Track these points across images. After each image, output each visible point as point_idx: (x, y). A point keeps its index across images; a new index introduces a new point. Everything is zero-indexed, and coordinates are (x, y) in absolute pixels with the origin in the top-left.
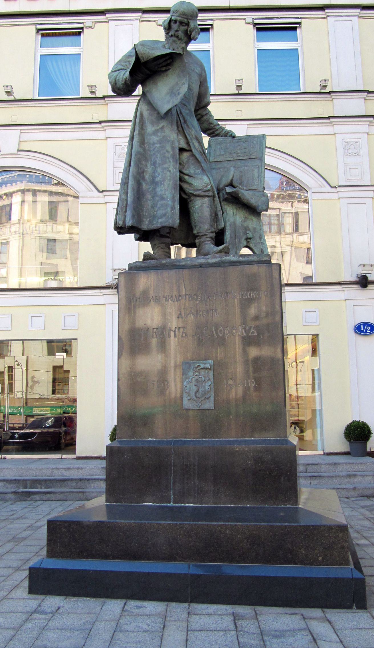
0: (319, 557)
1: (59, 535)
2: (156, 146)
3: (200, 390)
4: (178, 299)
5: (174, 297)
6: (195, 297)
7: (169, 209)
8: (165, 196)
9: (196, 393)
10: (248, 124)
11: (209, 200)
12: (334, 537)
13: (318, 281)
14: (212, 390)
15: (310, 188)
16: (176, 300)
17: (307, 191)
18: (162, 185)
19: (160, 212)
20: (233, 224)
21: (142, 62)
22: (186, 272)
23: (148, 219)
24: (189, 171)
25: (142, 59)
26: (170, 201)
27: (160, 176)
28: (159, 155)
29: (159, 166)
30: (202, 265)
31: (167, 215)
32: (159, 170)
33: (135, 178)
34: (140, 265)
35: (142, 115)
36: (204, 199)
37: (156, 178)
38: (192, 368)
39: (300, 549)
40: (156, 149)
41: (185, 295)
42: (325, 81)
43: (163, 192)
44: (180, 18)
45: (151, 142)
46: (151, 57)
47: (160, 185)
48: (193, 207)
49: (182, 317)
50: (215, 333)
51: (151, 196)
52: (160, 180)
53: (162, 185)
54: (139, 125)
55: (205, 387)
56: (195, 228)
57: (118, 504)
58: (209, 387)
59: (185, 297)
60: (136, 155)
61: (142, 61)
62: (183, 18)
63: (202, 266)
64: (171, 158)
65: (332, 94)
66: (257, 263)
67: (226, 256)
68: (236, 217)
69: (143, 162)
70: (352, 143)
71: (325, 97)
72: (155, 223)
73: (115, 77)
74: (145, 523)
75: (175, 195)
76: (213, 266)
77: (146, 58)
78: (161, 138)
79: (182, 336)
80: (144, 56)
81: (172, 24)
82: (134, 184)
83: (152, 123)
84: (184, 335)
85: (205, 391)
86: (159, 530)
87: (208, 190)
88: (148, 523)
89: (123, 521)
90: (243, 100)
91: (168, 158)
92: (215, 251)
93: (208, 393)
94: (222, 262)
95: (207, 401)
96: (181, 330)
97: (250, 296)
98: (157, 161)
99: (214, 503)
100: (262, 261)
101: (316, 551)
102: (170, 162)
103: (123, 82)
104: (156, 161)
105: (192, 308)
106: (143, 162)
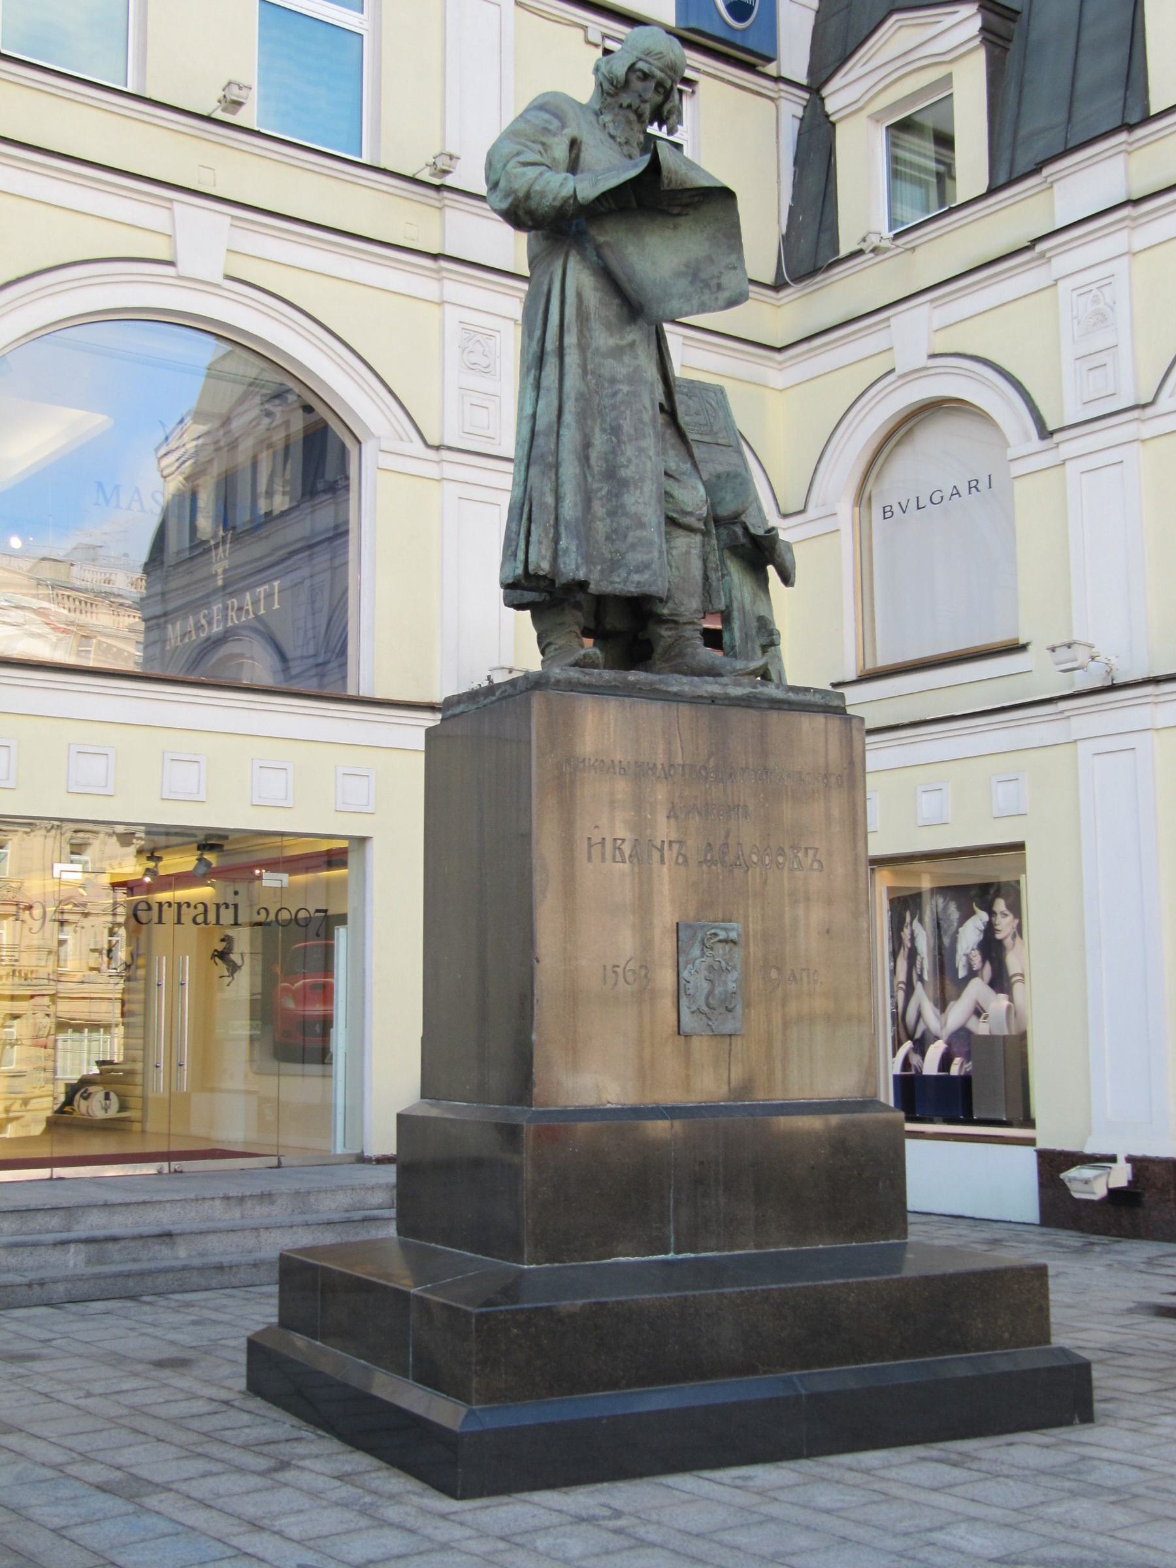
1: (503, 1347)
3: (716, 992)
4: (667, 771)
5: (659, 767)
6: (703, 773)
8: (645, 520)
9: (707, 998)
10: (233, 217)
15: (371, 435)
16: (663, 775)
17: (359, 442)
18: (639, 491)
19: (635, 558)
22: (684, 709)
23: (599, 567)
25: (666, 181)
27: (632, 467)
28: (628, 412)
30: (716, 698)
31: (653, 566)
34: (578, 678)
36: (692, 535)
37: (622, 469)
38: (699, 939)
41: (683, 766)
42: (240, 88)
45: (606, 372)
46: (688, 186)
49: (676, 818)
51: (604, 510)
53: (639, 491)
55: (725, 983)
59: (683, 770)
61: (665, 186)
63: (716, 702)
65: (446, 194)
66: (821, 709)
70: (479, 337)
71: (427, 196)
72: (617, 579)
73: (531, 181)
74: (694, 1296)
76: (738, 705)
79: (677, 863)
83: (608, 326)
84: (681, 860)
85: (726, 991)
88: (701, 1295)
89: (648, 1296)
90: (221, 140)
92: (741, 670)
93: (732, 997)
94: (755, 697)
95: (730, 1015)
96: (675, 847)
99: (758, 1246)
100: (831, 706)
101: (1000, 1322)
103: (557, 203)
104: (619, 427)
105: (697, 797)
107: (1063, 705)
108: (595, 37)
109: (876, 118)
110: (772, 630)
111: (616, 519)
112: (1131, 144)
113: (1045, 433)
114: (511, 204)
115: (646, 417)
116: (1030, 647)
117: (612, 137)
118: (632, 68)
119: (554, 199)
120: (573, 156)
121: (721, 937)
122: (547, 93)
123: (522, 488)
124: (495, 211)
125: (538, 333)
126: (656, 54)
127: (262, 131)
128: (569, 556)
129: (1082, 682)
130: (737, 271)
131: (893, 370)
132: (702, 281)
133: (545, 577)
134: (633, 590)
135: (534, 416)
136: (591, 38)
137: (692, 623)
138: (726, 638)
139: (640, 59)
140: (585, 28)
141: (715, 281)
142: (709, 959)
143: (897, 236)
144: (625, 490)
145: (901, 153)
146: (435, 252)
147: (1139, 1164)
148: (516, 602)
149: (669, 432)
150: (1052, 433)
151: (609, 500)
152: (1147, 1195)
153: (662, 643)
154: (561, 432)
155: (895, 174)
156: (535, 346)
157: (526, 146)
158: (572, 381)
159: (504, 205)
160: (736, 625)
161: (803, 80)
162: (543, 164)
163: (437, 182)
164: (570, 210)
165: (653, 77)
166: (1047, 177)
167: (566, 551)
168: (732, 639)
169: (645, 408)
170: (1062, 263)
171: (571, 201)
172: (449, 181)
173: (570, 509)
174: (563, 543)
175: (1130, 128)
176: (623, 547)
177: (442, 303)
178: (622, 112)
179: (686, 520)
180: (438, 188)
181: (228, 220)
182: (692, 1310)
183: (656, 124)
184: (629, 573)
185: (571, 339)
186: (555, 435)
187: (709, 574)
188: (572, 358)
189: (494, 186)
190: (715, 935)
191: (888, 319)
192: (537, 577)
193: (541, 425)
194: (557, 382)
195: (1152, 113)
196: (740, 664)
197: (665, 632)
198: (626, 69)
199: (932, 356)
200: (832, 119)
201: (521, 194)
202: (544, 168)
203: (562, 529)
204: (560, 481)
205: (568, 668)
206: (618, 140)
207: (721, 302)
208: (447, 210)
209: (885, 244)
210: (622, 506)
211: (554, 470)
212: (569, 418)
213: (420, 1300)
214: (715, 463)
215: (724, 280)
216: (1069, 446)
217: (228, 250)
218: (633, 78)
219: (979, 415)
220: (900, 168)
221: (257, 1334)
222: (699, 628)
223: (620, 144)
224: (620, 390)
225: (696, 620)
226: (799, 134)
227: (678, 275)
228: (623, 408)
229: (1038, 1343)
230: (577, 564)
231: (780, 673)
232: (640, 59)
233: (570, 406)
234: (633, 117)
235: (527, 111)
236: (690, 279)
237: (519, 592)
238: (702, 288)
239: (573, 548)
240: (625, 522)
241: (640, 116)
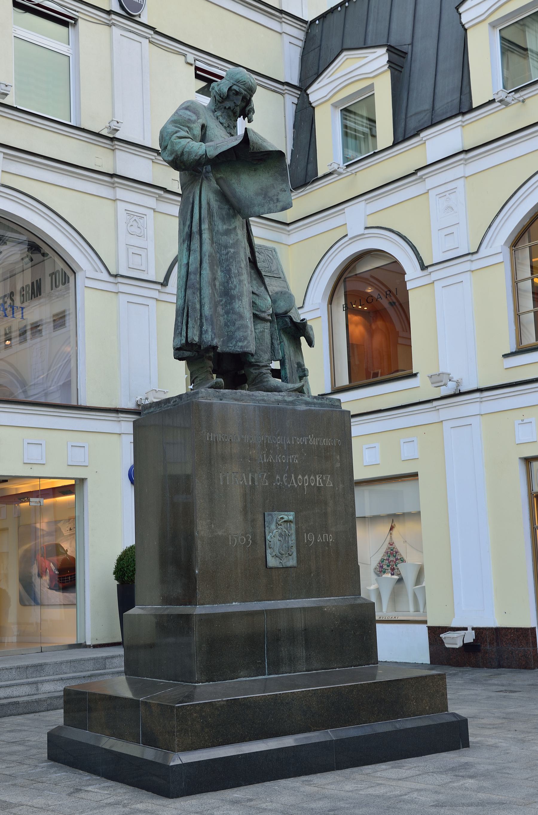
0: (426, 706)
1: (190, 723)
12: (436, 686)
13: (89, 404)
17: (75, 273)
25: (252, 148)
39: (412, 701)
42: (118, 123)
44: (246, 93)
46: (262, 150)
50: (294, 482)
51: (224, 311)
55: (288, 542)
57: (211, 683)
83: (223, 219)
86: (293, 700)
92: (291, 388)
93: (291, 548)
97: (326, 444)
103: (197, 158)
107: (435, 403)
108: (190, 59)
109: (335, 105)
110: (304, 369)
112: (463, 122)
113: (423, 267)
114: (174, 158)
115: (243, 265)
116: (418, 375)
117: (221, 123)
118: (230, 89)
119: (195, 156)
120: (203, 133)
121: (285, 519)
122: (189, 101)
123: (183, 301)
124: (165, 161)
125: (188, 223)
126: (242, 82)
127: (18, 107)
128: (208, 333)
129: (444, 391)
130: (286, 192)
131: (346, 235)
133: (196, 344)
134: (239, 350)
135: (188, 264)
136: (189, 61)
137: (267, 366)
138: (283, 373)
139: (234, 84)
140: (185, 55)
141: (276, 197)
142: (280, 530)
143: (348, 166)
145: (349, 123)
146: (111, 173)
147: (478, 630)
148: (180, 357)
149: (253, 271)
150: (427, 267)
151: (226, 306)
152: (483, 646)
153: (252, 376)
154: (202, 272)
155: (346, 134)
156: (187, 229)
157: (181, 128)
158: (207, 247)
159: (170, 159)
160: (287, 366)
161: (295, 81)
162: (189, 138)
163: (111, 136)
164: (203, 161)
165: (241, 93)
166: (422, 138)
167: (206, 331)
168: (286, 373)
169: (242, 260)
170: (431, 182)
171: (204, 156)
172: (118, 135)
173: (207, 310)
174: (204, 328)
175: (464, 114)
176: (233, 328)
177: (115, 200)
178: (226, 111)
179: (263, 315)
180: (112, 139)
181: (2, 155)
182: (279, 701)
183: (242, 117)
184: (236, 342)
185: (205, 226)
186: (199, 274)
187: (273, 341)
188: (206, 236)
189: (165, 148)
190: (282, 518)
191: (343, 209)
192: (192, 345)
193: (191, 269)
194: (199, 247)
195: (474, 106)
196: (290, 386)
197: (254, 372)
198: (227, 89)
199: (366, 228)
200: (313, 105)
201: (179, 153)
202: (190, 139)
203: (204, 321)
204: (202, 297)
205: (208, 389)
206: (224, 125)
207: (279, 208)
208: (117, 152)
209: (340, 170)
210: (233, 309)
211: (199, 291)
212: (205, 265)
213: (145, 703)
214: (273, 286)
215: (280, 197)
216: (436, 274)
217: (2, 171)
218: (231, 93)
219: (388, 257)
220: (349, 131)
221: (53, 730)
222: (270, 368)
223: (225, 128)
225: (268, 365)
226: (296, 112)
227: (257, 194)
229: (443, 711)
230: (212, 337)
231: (308, 390)
232: (234, 84)
234: (231, 114)
235: (179, 110)
236: (263, 196)
237: (182, 352)
238: (269, 201)
240: (235, 317)
241: (234, 113)
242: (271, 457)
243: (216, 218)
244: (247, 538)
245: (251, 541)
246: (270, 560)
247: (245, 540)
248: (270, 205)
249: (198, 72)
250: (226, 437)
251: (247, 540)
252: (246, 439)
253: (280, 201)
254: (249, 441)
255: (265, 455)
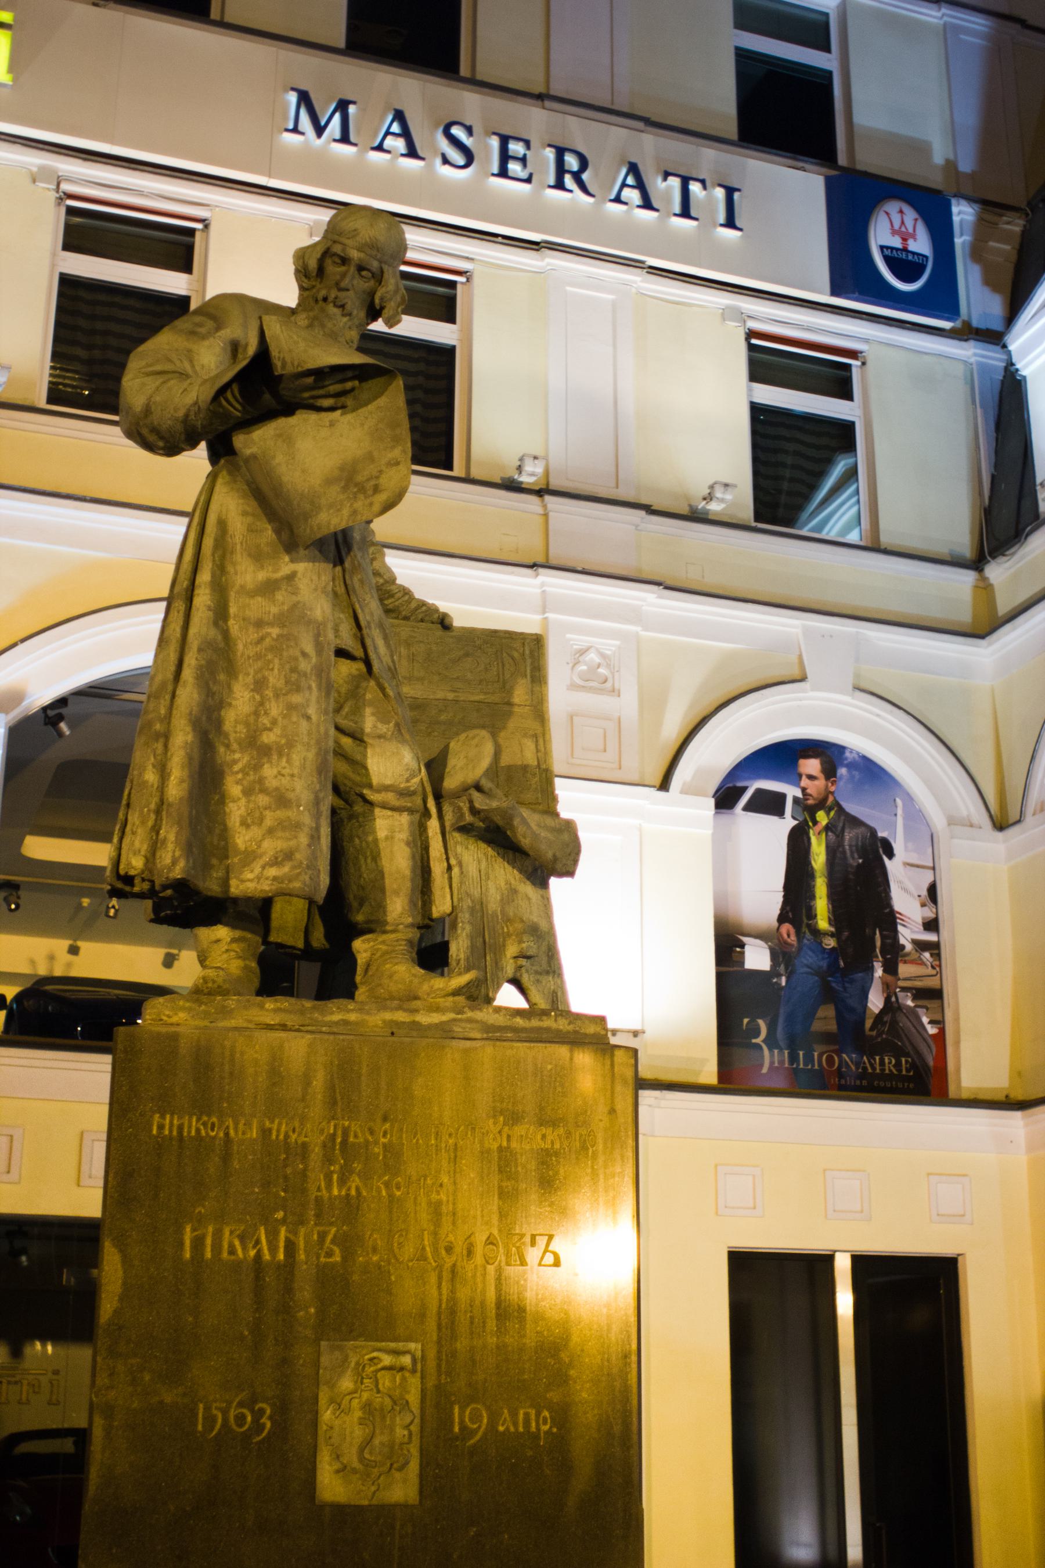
2: (269, 630)
3: (376, 1441)
7: (303, 839)
8: (291, 795)
9: (361, 1450)
11: (411, 823)
14: (416, 1440)
18: (284, 760)
20: (478, 907)
21: (276, 374)
24: (356, 723)
26: (306, 813)
27: (277, 731)
28: (276, 661)
29: (277, 696)
32: (275, 709)
33: (196, 724)
35: (222, 524)
38: (353, 1365)
40: (267, 640)
43: (285, 781)
44: (362, 255)
47: (275, 757)
48: (359, 837)
51: (240, 788)
52: (277, 743)
53: (284, 760)
54: (213, 555)
55: (392, 1430)
56: (361, 905)
58: (406, 1433)
60: (200, 650)
62: (371, 256)
64: (314, 678)
67: (472, 1009)
68: (487, 885)
69: (222, 677)
75: (321, 795)
77: (293, 364)
78: (286, 608)
80: (288, 360)
81: (328, 262)
82: (192, 742)
87: (413, 791)
91: (305, 675)
95: (397, 1475)
98: (271, 679)
102: (310, 688)
106: (222, 677)
111: (253, 798)
132: (356, 485)
134: (267, 888)
141: (372, 483)
144: (265, 760)
154: (178, 692)
167: (164, 841)
186: (168, 697)
210: (261, 781)
224: (269, 634)
227: (329, 482)
228: (270, 657)
230: (173, 856)
233: (191, 660)
239: (172, 837)
242: (355, 1182)
243: (239, 556)
244: (258, 1414)
245: (268, 1425)
246: (326, 1481)
247: (249, 1419)
248: (355, 505)
249: (754, 341)
250: (213, 1125)
251: (256, 1420)
252: (278, 1131)
253: (380, 491)
254: (287, 1136)
255: (335, 1177)
